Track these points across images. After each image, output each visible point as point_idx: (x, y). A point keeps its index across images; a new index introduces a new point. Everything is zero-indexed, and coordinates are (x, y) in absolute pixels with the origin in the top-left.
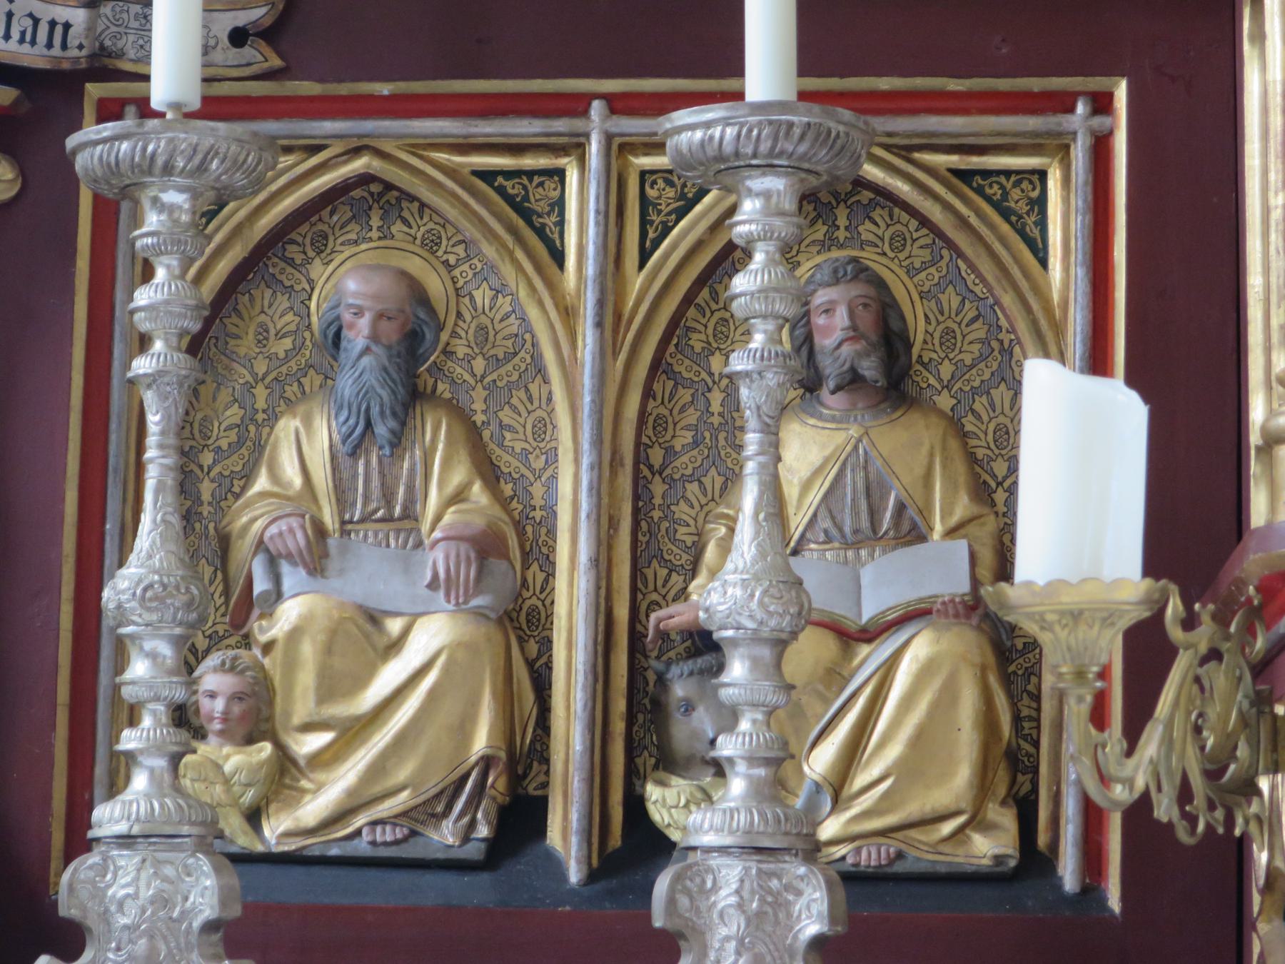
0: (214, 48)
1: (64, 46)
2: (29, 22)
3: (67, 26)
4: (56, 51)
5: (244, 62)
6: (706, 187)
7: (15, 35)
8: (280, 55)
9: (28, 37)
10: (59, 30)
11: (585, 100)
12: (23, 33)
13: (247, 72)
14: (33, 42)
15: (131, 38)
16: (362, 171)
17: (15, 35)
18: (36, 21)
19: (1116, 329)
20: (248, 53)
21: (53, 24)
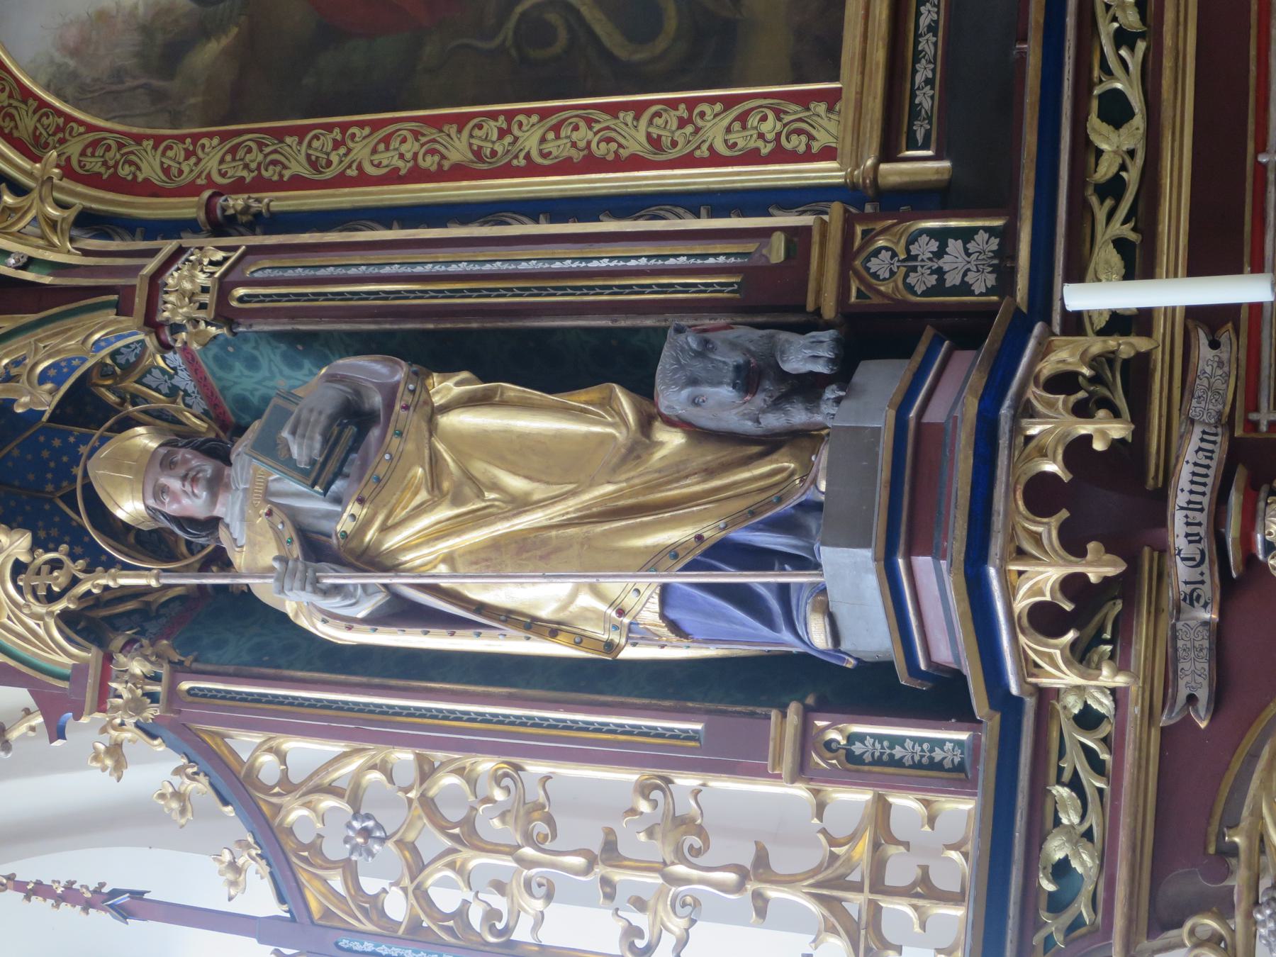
0: (1220, 358)
1: (1216, 435)
2: (1200, 453)
3: (1194, 474)
4: (1218, 439)
5: (1229, 342)
6: (243, 423)
7: (1207, 462)
8: (1227, 322)
9: (1209, 454)
10: (1206, 437)
11: (1257, 164)
12: (1207, 457)
13: (1234, 340)
14: (1212, 452)
15: (1211, 407)
16: (781, 212)
17: (1207, 462)
18: (1200, 449)
19: (1164, 164)
20: (1224, 339)
21: (1202, 440)
